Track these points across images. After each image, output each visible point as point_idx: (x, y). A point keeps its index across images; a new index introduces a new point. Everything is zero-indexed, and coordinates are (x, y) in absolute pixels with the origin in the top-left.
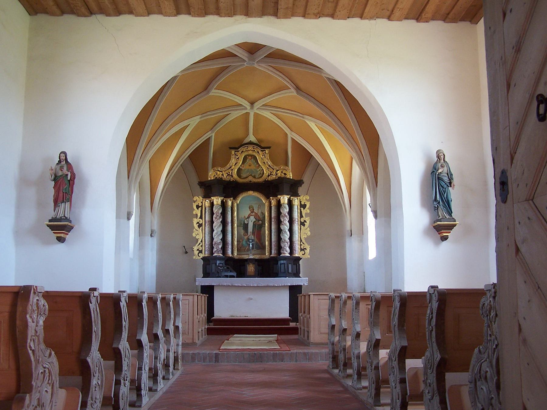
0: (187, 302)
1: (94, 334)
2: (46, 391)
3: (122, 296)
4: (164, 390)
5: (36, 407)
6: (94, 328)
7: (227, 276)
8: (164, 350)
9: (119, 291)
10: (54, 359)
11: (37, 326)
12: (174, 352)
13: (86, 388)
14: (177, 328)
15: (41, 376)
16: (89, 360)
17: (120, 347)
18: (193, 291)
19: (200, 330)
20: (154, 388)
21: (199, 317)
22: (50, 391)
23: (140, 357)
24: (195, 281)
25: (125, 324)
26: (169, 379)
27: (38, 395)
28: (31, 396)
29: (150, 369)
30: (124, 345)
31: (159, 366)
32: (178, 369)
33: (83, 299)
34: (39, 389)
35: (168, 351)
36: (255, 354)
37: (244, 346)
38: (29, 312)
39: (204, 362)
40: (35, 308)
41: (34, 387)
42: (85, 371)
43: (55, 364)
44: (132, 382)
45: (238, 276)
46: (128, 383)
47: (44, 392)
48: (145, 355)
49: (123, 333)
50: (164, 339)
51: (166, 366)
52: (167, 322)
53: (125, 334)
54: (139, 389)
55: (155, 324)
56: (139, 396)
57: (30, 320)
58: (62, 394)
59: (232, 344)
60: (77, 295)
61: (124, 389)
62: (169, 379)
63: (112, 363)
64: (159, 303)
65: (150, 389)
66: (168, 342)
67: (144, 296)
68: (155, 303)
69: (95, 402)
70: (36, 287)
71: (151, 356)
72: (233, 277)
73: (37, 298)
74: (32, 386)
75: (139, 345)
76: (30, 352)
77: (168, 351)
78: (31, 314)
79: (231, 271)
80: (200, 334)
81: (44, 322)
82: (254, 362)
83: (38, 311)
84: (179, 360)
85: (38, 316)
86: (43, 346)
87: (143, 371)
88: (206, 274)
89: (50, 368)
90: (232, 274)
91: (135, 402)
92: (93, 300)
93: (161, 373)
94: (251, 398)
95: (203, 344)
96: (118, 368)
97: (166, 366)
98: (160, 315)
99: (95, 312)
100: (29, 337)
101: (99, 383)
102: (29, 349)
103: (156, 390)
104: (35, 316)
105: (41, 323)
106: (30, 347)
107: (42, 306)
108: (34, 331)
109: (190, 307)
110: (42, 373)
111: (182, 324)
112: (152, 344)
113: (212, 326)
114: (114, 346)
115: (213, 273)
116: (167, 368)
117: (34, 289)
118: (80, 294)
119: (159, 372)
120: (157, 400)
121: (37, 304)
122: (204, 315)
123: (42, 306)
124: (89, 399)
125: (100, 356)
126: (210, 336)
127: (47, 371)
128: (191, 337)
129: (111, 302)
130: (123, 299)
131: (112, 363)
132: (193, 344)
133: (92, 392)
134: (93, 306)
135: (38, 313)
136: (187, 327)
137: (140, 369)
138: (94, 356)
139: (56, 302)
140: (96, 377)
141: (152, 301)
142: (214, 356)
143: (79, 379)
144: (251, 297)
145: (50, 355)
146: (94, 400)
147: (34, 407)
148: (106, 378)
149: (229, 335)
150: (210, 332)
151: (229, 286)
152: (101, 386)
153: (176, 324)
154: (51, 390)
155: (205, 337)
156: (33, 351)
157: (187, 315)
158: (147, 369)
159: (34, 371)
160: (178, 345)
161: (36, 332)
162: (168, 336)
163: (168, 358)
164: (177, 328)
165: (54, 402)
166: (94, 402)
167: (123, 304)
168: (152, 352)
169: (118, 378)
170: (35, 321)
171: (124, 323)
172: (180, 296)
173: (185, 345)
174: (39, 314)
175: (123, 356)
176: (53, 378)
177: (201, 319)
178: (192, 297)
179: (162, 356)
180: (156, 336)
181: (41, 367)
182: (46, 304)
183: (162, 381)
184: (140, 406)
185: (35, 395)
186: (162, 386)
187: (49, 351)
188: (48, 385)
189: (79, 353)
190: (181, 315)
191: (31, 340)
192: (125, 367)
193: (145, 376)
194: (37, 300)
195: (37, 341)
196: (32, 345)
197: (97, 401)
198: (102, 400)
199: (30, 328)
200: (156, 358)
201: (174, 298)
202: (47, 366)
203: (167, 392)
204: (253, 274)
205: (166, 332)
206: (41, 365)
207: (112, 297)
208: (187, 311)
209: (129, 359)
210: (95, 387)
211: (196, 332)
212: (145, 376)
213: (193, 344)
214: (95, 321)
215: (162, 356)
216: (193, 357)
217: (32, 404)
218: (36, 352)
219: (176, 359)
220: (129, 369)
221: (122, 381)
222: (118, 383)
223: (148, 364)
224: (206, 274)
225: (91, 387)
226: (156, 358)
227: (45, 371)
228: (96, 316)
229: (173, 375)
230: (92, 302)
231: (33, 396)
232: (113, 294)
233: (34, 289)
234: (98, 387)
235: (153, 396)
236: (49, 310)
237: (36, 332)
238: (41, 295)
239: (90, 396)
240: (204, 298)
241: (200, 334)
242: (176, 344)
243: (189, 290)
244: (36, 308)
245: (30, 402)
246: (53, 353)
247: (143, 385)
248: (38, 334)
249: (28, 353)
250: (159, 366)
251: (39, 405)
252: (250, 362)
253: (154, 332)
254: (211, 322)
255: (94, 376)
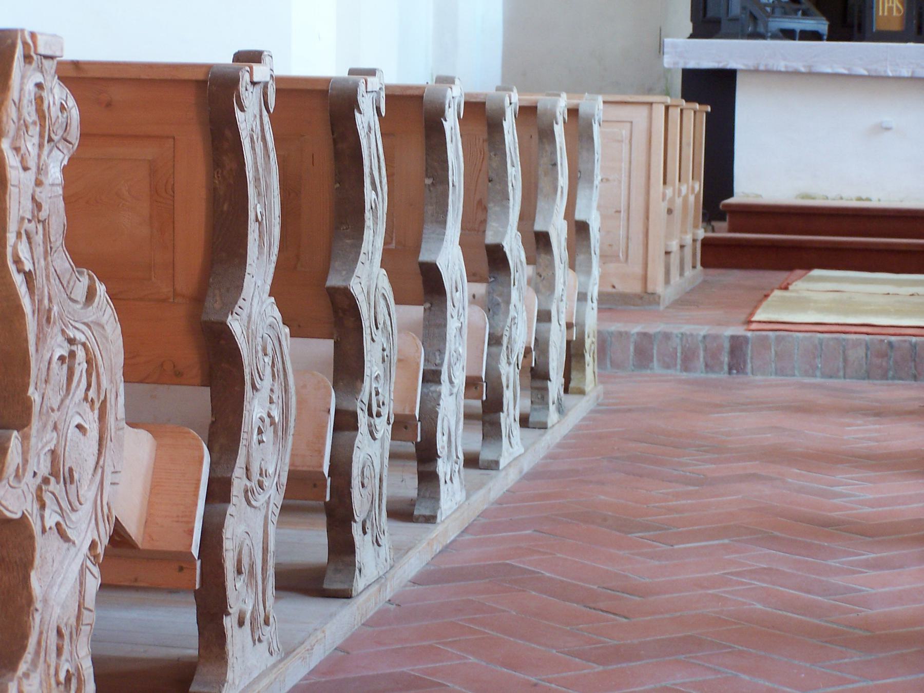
0: (625, 132)
1: (253, 227)
2: (79, 427)
3: (361, 89)
4: (527, 465)
5: (46, 481)
6: (255, 206)
7: (789, 34)
8: (529, 312)
9: (352, 72)
10: (104, 311)
11: (39, 183)
12: (569, 326)
13: (224, 433)
14: (580, 230)
15: (59, 372)
16: (236, 325)
17: (357, 288)
18: (650, 91)
19: (674, 246)
20: (486, 455)
21: (669, 192)
22: (91, 422)
23: (433, 332)
24: (661, 49)
25: (376, 198)
26: (543, 426)
27: (50, 439)
28: (25, 438)
29: (472, 383)
30: (368, 279)
31: (509, 373)
32: (582, 392)
33: (212, 93)
34: (55, 416)
35: (544, 316)
36: (890, 344)
37: (847, 313)
38: (11, 128)
39: (686, 369)
40: (30, 114)
41: (36, 409)
42: (220, 367)
43: (109, 328)
44: (401, 425)
45: (835, 35)
46: (384, 428)
47: (72, 432)
48: (452, 325)
49: (368, 234)
50: (529, 270)
51: (536, 375)
52: (541, 204)
53: (374, 238)
54: (426, 454)
55: (493, 208)
56: (428, 479)
57: (12, 160)
58: (137, 449)
59: (802, 304)
60: (186, 76)
61: (371, 450)
62: (543, 426)
63: (324, 348)
64: (509, 125)
65: (472, 461)
66: (543, 283)
67: (449, 94)
68: (495, 127)
69: (261, 485)
70: (33, 35)
71: (474, 332)
72: (815, 36)
73: (39, 78)
74: (27, 406)
75: (431, 286)
76: (18, 280)
77: (544, 316)
78: (17, 137)
79: (806, 14)
80: (675, 259)
81: (65, 170)
82: (885, 377)
83: (42, 126)
84: (588, 358)
85: (41, 146)
86: (62, 261)
87: (445, 388)
88: (706, 25)
89: (92, 344)
90: (809, 24)
91: (412, 503)
92: (251, 98)
93: (514, 403)
94: (867, 510)
95: (684, 302)
96: (348, 368)
97: (536, 375)
98: (514, 173)
99: (259, 145)
100: (12, 227)
101: (276, 414)
102: (12, 268)
103: (493, 465)
104: (30, 145)
105: (55, 174)
106: (18, 261)
107: (55, 111)
108: (28, 205)
109: (630, 179)
110: (62, 358)
111: (604, 217)
112: (480, 289)
113: (722, 231)
114: (334, 281)
115: (735, 20)
116: (539, 384)
117: (25, 44)
118: (200, 76)
119: (508, 395)
120: (500, 502)
121: (39, 100)
122: (693, 189)
123: (55, 111)
124: (238, 471)
125: (278, 315)
126: (711, 271)
127: (81, 354)
128: (638, 270)
129: (321, 112)
130: (366, 103)
131: (324, 348)
132: (645, 299)
133: (248, 447)
134: (251, 120)
135: (41, 136)
136: (622, 232)
137: (432, 377)
138: (255, 315)
139: (109, 105)
140: (264, 393)
141: (481, 116)
142: (727, 345)
143: (198, 399)
144: (887, 118)
145: (91, 295)
146: (255, 476)
147: (39, 480)
148: (299, 402)
149: (790, 268)
150: (714, 254)
151: (796, 73)
152: (280, 429)
153: (579, 216)
154: (95, 426)
155: (694, 274)
156: (29, 277)
157: (624, 186)
158: (460, 380)
159: (32, 349)
160: (582, 297)
161: (38, 206)
162: (543, 258)
163: (542, 344)
164: (580, 230)
165: (108, 470)
166: (254, 484)
167: (367, 120)
168: (480, 316)
169: (346, 405)
170: (32, 163)
171: (369, 195)
172: (594, 105)
173: (610, 302)
174: (46, 139)
175: (366, 324)
176: (105, 383)
177: (679, 201)
178: (643, 111)
179: (521, 334)
180: (496, 259)
181: (60, 338)
182: (71, 102)
183: (517, 429)
184: (431, 519)
185: (41, 439)
186: (517, 451)
187: (85, 281)
188: (86, 406)
189: (199, 299)
190: (597, 181)
191: (19, 235)
192: (373, 365)
193: (451, 406)
194: (39, 86)
195: (39, 238)
196: (24, 251)
197: (266, 483)
198: (284, 480)
199: (12, 191)
200: (495, 340)
201: (573, 112)
202: (80, 337)
203: (534, 475)
204: (896, 26)
205: (540, 243)
206: (56, 330)
207: (324, 93)
208: (624, 166)
209: (389, 337)
210: (260, 432)
211: (657, 253)
212: (451, 406)
213: (645, 299)
214: (257, 180)
215: (521, 334)
216: (644, 353)
217: (32, 466)
218: (40, 280)
219: (574, 353)
220: (388, 372)
221: (363, 419)
222: (346, 422)
223: (463, 362)
224: (706, 25)
225: (245, 427)
226: (495, 340)
227: (72, 354)
228: (260, 161)
229: (561, 410)
230: (246, 103)
231: (33, 441)
232: (327, 81)
233: (25, 44)
234: (268, 436)
235: (481, 486)
236: (84, 135)
237: (38, 206)
238: (50, 66)
239: (241, 461)
240: (693, 119)
241: (675, 259)
242: (574, 296)
243: (631, 82)
244: (34, 117)
245: (25, 461)
246: (101, 289)
247: (441, 442)
248: (43, 215)
249: (12, 284)
250: (509, 373)
251: (55, 473)
252: (868, 376)
253: (490, 239)
254: (721, 217)
255: (254, 387)
